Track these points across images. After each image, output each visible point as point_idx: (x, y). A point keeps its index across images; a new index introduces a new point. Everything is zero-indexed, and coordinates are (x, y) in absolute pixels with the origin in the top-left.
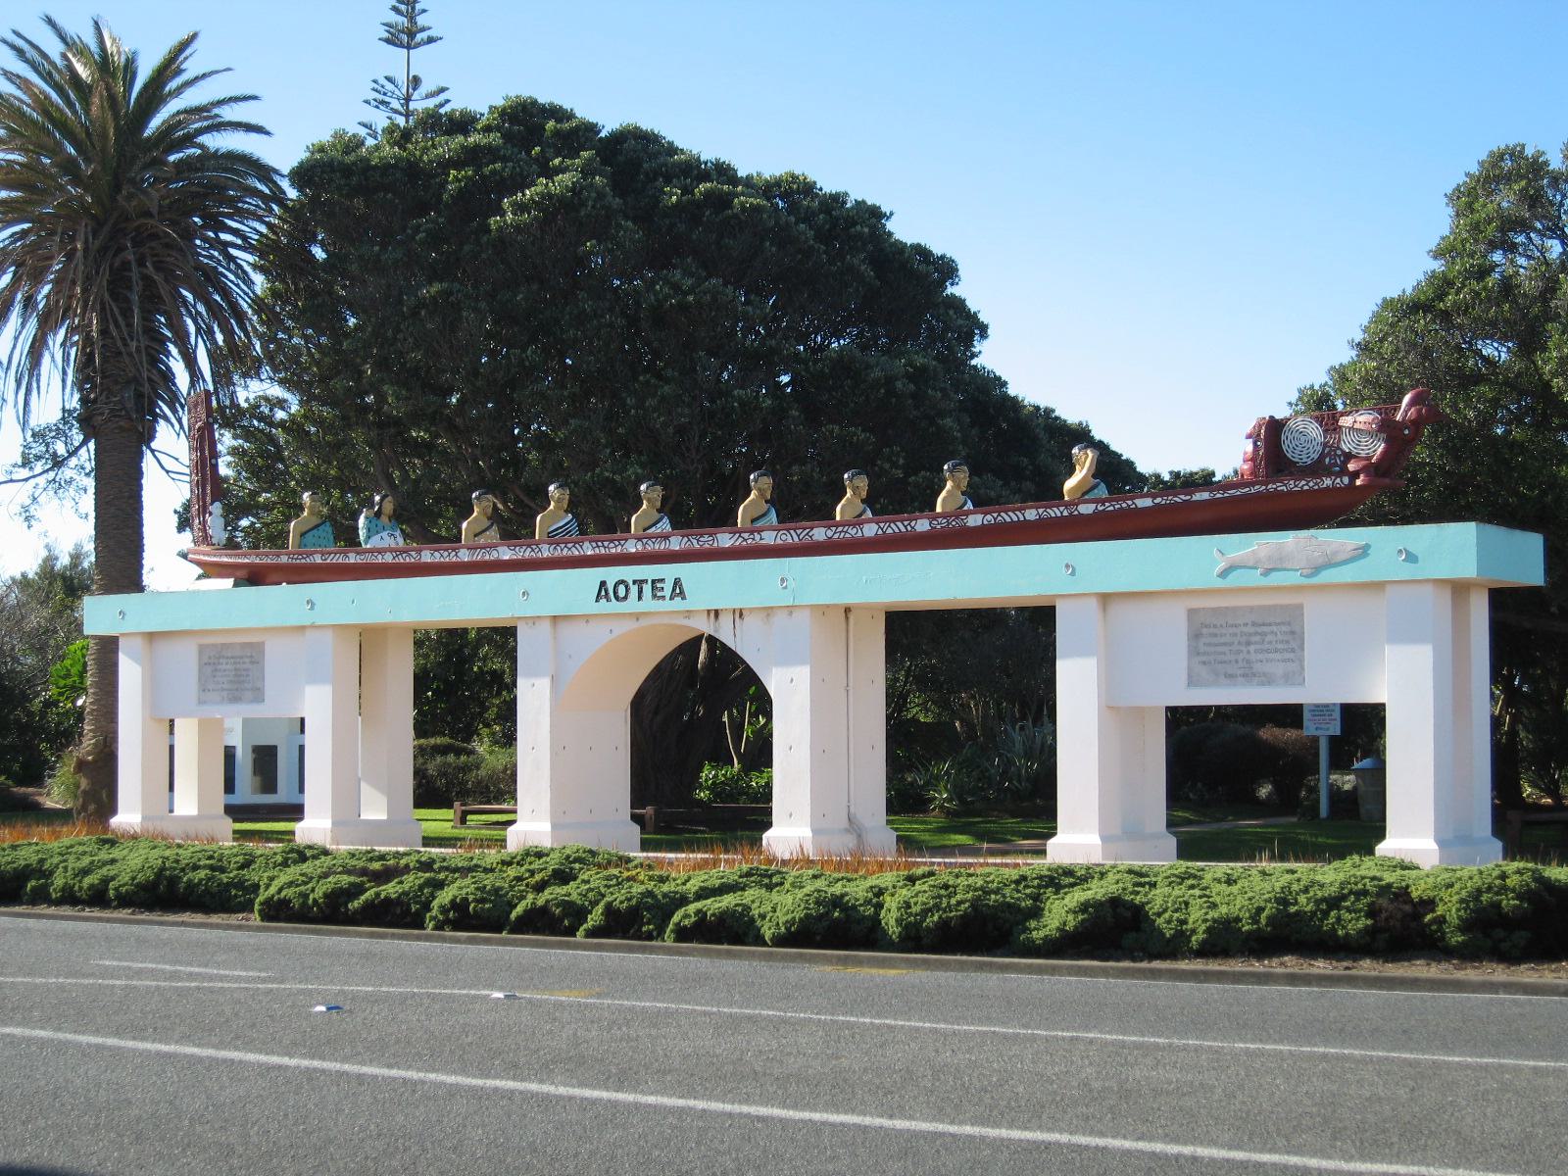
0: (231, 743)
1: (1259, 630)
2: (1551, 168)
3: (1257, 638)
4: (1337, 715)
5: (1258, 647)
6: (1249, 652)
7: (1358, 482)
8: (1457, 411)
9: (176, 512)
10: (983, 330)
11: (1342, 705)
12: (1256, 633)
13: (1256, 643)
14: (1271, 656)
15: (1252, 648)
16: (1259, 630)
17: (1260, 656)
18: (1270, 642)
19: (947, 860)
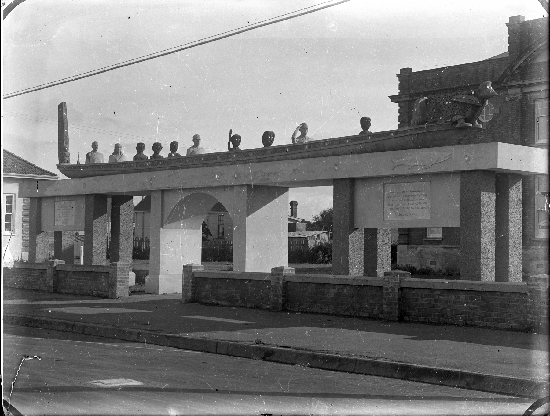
0: (371, 226)
1: (412, 194)
2: (418, 269)
3: (411, 198)
4: (203, 262)
5: (412, 202)
6: (408, 204)
7: (345, 291)
8: (37, 273)
9: (394, 99)
10: (392, 102)
11: (202, 261)
12: (412, 196)
13: (411, 200)
14: (417, 206)
15: (410, 202)
16: (412, 194)
17: (413, 206)
18: (417, 200)
19: (324, 354)
